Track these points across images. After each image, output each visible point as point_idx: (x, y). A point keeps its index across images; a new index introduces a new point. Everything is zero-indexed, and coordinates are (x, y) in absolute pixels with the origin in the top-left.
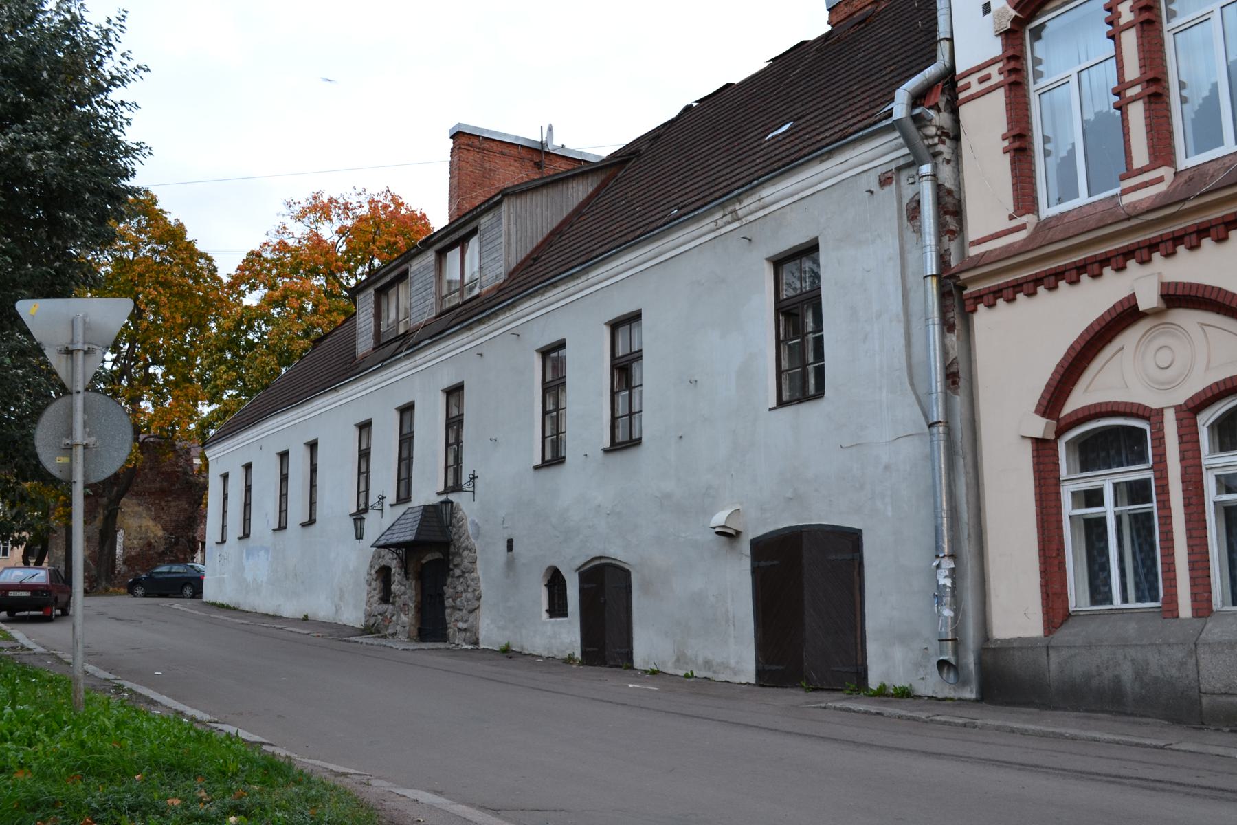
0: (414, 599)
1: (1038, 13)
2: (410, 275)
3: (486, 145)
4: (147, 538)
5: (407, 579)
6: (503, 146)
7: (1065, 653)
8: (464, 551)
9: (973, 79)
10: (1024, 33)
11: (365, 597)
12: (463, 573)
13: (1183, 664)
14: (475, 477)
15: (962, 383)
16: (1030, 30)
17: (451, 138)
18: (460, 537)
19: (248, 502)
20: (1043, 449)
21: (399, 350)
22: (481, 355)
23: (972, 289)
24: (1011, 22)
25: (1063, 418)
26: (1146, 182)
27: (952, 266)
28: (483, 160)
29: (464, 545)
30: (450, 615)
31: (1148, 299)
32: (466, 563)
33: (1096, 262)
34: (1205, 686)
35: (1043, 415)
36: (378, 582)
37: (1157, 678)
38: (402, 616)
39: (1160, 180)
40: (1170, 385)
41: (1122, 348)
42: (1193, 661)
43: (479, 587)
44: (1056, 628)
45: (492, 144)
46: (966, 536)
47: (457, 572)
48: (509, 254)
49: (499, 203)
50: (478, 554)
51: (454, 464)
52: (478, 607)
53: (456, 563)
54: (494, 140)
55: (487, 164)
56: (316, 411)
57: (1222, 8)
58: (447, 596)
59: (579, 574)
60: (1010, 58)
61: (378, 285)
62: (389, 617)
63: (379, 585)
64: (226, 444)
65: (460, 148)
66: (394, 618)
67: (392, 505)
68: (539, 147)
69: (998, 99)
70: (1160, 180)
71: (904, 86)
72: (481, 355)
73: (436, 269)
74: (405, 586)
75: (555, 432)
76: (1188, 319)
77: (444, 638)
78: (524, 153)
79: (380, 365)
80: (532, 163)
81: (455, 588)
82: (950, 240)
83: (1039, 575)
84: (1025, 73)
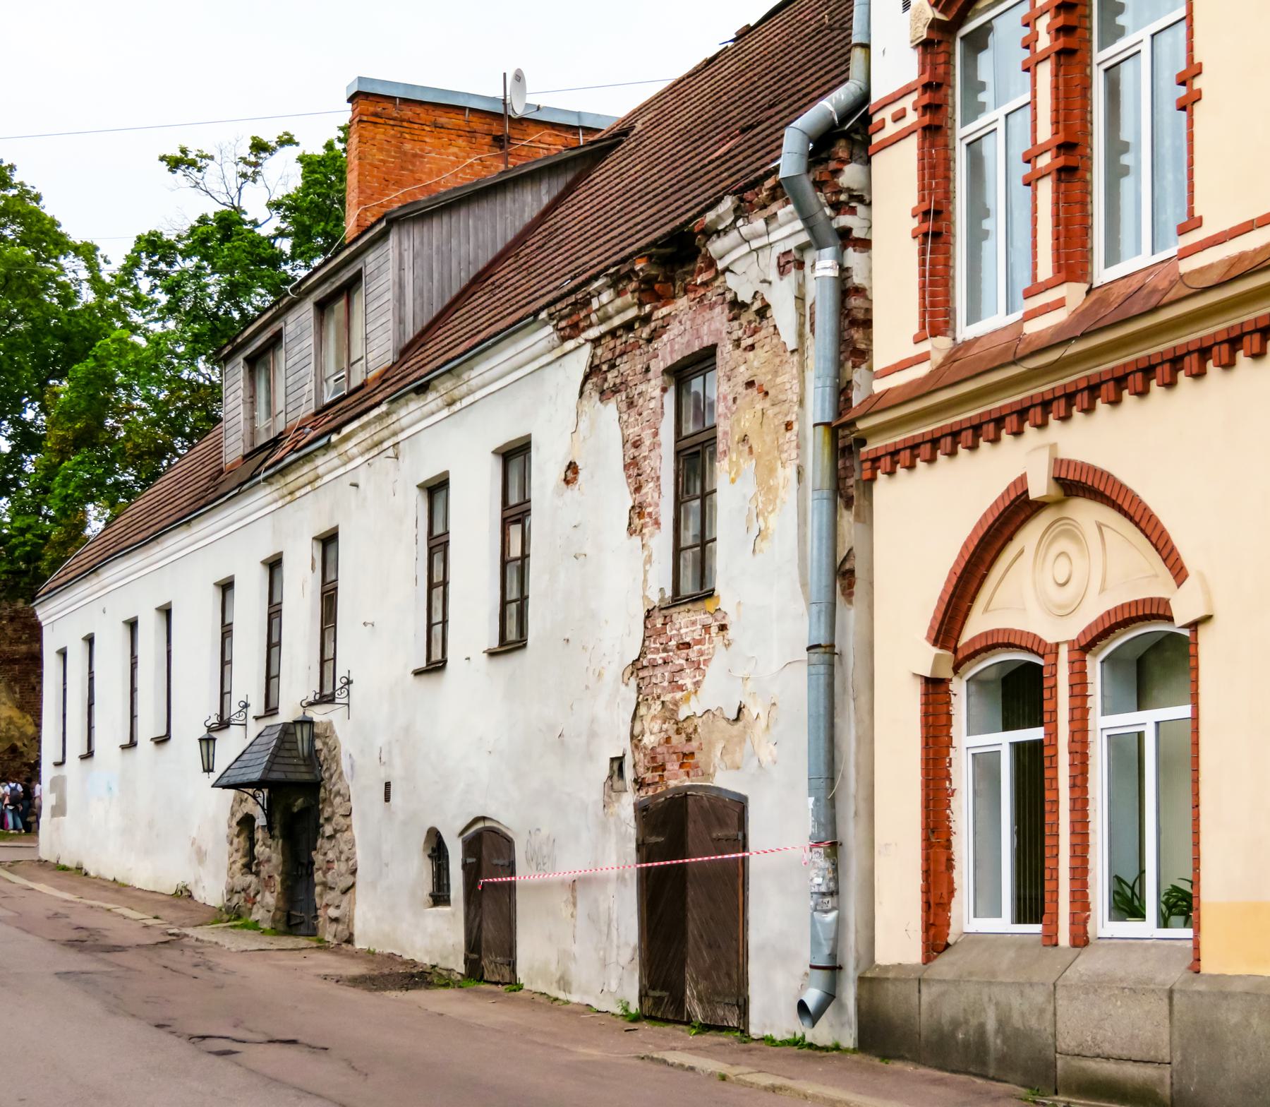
0: (280, 868)
1: (969, 14)
2: (286, 339)
3: (408, 112)
4: (10, 738)
5: (272, 837)
6: (438, 112)
7: (936, 989)
8: (335, 796)
9: (887, 114)
10: (955, 40)
11: (226, 862)
12: (336, 831)
13: (1042, 1011)
14: (349, 682)
15: (858, 588)
16: (962, 38)
17: (350, 100)
18: (331, 776)
19: (275, 640)
20: (935, 688)
21: (257, 472)
22: (356, 485)
23: (875, 445)
24: (929, 27)
25: (961, 647)
26: (1047, 305)
27: (854, 405)
28: (401, 137)
29: (335, 789)
30: (321, 895)
31: (1039, 488)
32: (338, 819)
33: (1138, 370)
34: (1062, 1045)
35: (935, 643)
36: (242, 838)
37: (1018, 1029)
38: (267, 894)
39: (1060, 304)
40: (1067, 612)
41: (1022, 552)
42: (1051, 1008)
43: (355, 853)
44: (940, 953)
45: (419, 110)
46: (852, 813)
47: (328, 830)
48: (401, 321)
49: (384, 235)
50: (353, 803)
51: (326, 661)
52: (353, 885)
53: (326, 815)
54: (421, 103)
55: (407, 147)
56: (127, 576)
57: (1153, 36)
58: (316, 866)
59: (464, 842)
60: (927, 87)
61: (248, 352)
62: (252, 895)
63: (243, 844)
64: (62, 600)
65: (360, 121)
66: (259, 898)
67: (257, 718)
68: (499, 109)
69: (910, 149)
70: (1060, 304)
71: (797, 123)
72: (356, 485)
73: (316, 333)
74: (270, 847)
75: (698, 542)
76: (1085, 513)
77: (312, 932)
78: (478, 124)
79: (236, 491)
80: (488, 139)
81: (325, 854)
82: (854, 367)
83: (920, 876)
84: (950, 110)
